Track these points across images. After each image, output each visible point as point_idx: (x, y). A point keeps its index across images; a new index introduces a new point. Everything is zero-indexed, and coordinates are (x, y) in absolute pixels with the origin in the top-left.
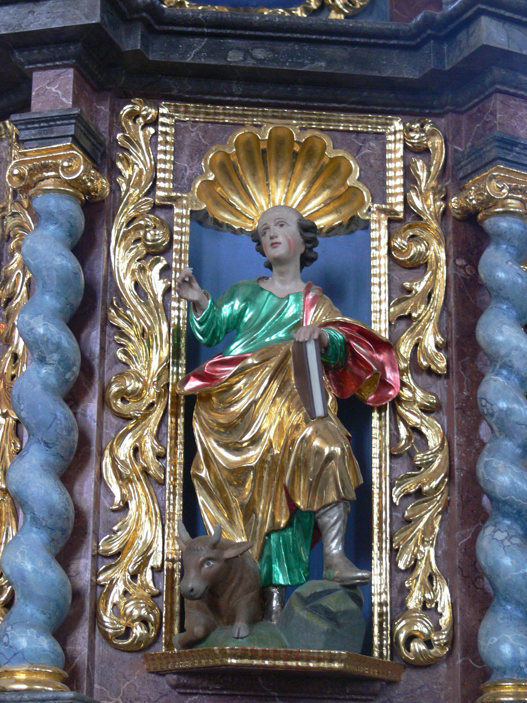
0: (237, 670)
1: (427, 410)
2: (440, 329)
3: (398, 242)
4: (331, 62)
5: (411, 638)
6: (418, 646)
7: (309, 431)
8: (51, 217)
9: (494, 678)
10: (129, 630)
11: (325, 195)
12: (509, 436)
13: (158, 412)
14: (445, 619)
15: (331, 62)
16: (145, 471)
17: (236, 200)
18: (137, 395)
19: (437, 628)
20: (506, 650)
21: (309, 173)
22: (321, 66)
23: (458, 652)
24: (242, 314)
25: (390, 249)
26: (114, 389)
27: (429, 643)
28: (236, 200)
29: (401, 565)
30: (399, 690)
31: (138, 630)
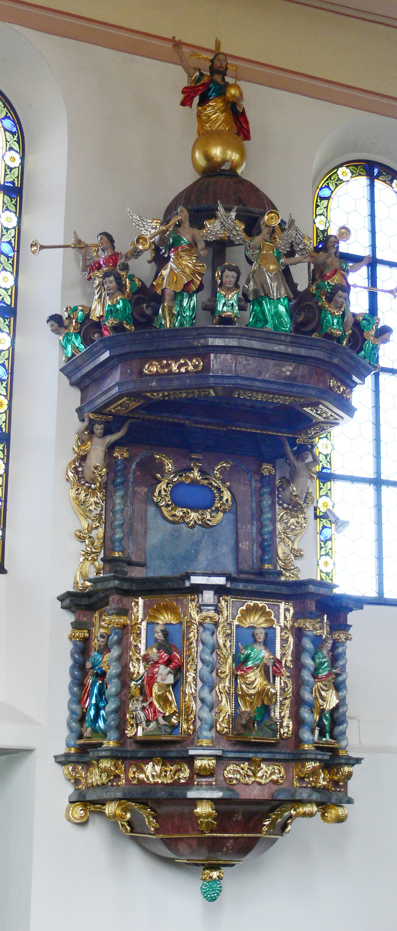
0: (254, 742)
1: (288, 677)
2: (292, 656)
3: (283, 634)
4: (271, 589)
5: (284, 733)
6: (286, 735)
7: (269, 687)
8: (209, 630)
9: (303, 743)
10: (223, 730)
11: (264, 618)
12: (308, 686)
13: (229, 676)
14: (291, 729)
15: (271, 589)
16: (226, 691)
17: (244, 621)
18: (224, 672)
19: (289, 730)
20: (306, 736)
21: (260, 613)
22: (269, 591)
23: (294, 736)
24: (250, 654)
25: (281, 636)
26: (219, 671)
27: (287, 734)
28: (244, 621)
29: (282, 715)
30: (280, 745)
31: (226, 730)
